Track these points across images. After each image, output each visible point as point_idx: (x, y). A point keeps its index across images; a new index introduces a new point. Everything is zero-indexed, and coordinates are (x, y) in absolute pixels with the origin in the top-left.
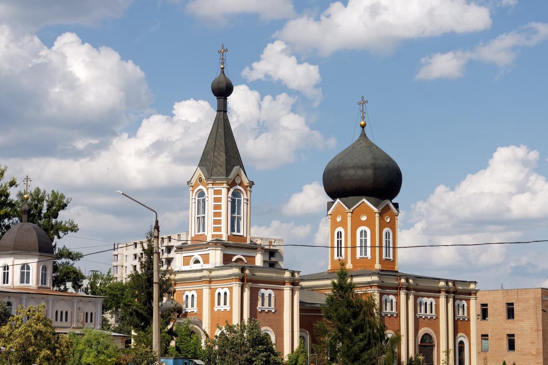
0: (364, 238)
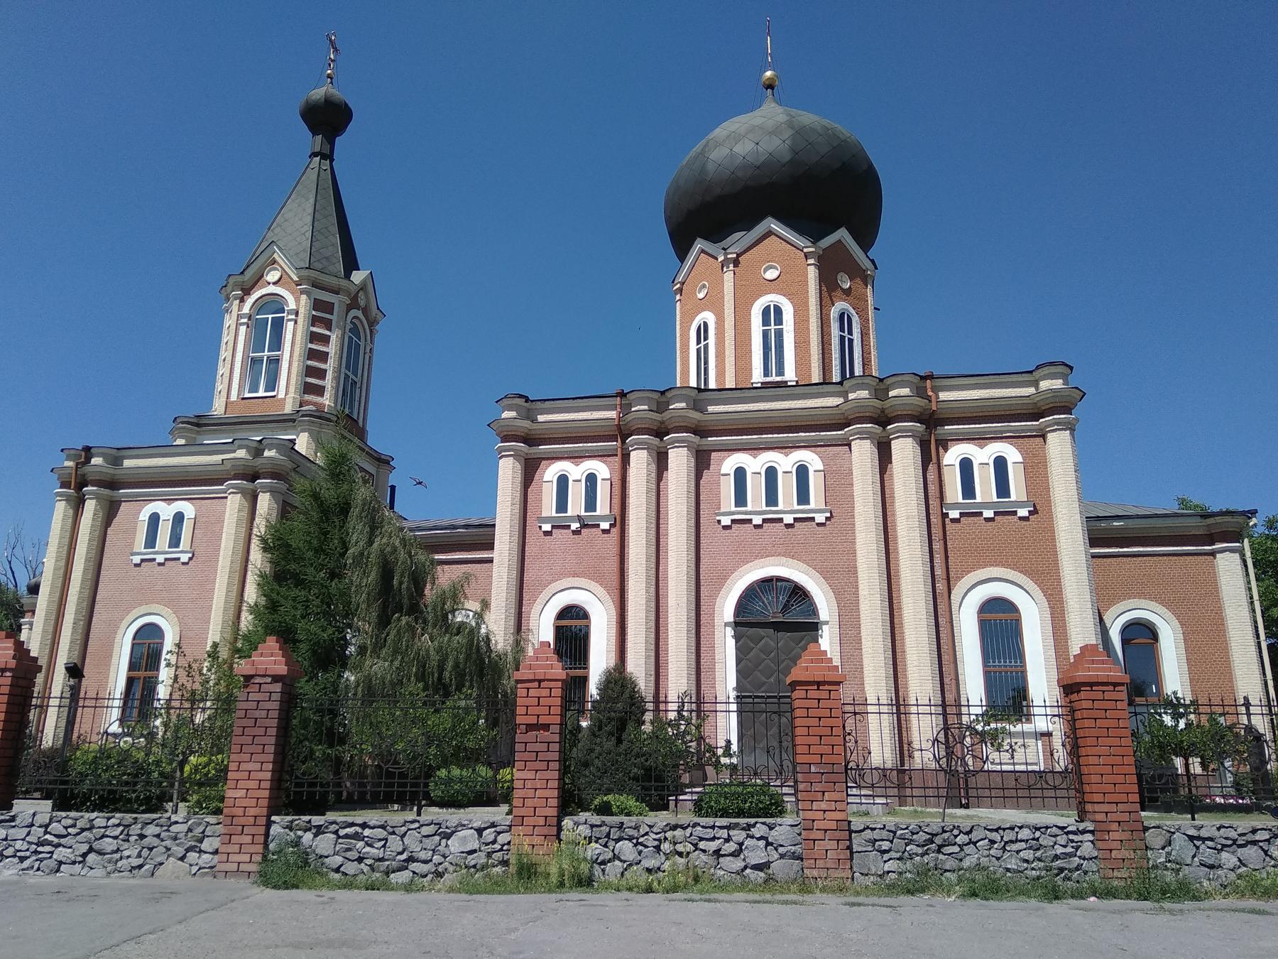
0: (773, 327)
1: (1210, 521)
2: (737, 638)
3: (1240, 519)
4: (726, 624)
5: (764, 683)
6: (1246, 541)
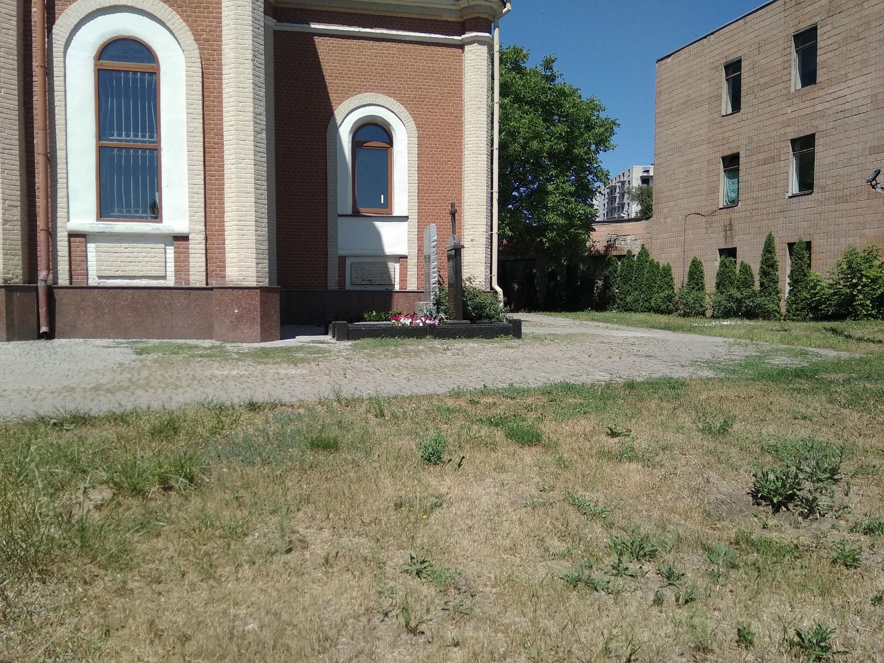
6: (497, 32)
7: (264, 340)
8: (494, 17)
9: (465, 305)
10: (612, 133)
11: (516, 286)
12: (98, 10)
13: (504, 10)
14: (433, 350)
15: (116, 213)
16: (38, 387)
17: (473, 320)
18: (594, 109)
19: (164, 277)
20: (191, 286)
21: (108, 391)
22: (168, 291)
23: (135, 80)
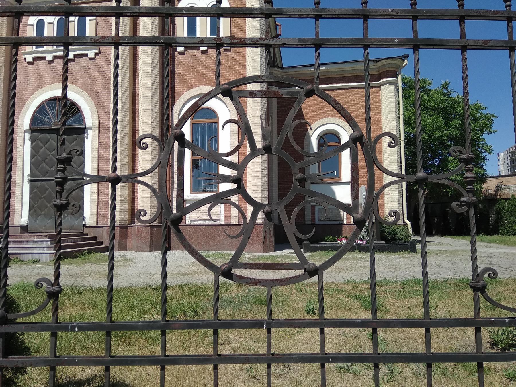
1: (379, 64)
2: (32, 140)
3: (398, 62)
4: (25, 132)
5: (48, 171)
6: (400, 77)
7: (265, 251)
8: (398, 69)
9: (383, 232)
10: (492, 122)
11: (436, 219)
12: (193, 97)
13: (404, 65)
14: (355, 258)
15: (199, 190)
16: (154, 273)
17: (388, 241)
18: (479, 109)
19: (219, 220)
20: (231, 224)
21: (183, 275)
22: (221, 227)
23: (208, 126)
